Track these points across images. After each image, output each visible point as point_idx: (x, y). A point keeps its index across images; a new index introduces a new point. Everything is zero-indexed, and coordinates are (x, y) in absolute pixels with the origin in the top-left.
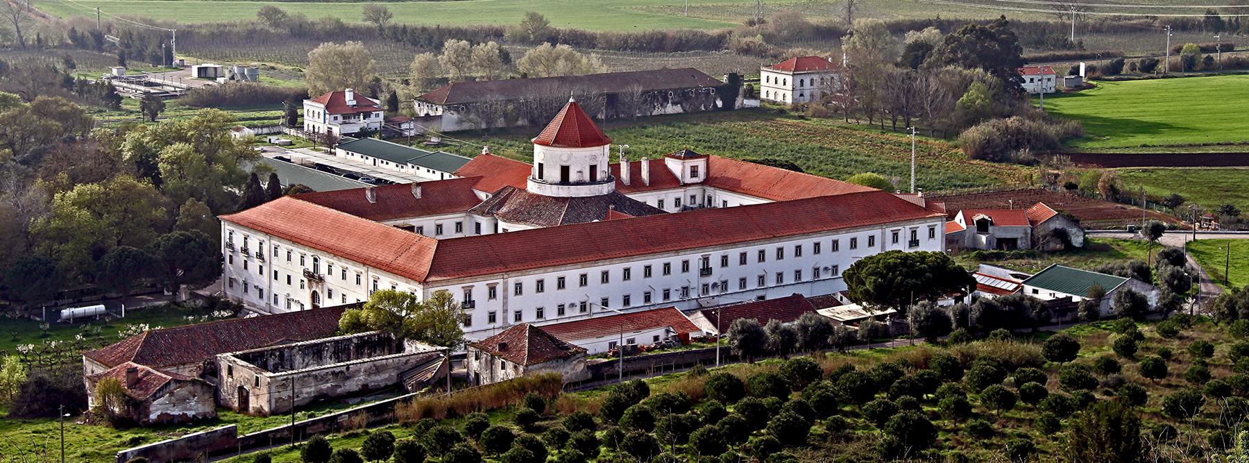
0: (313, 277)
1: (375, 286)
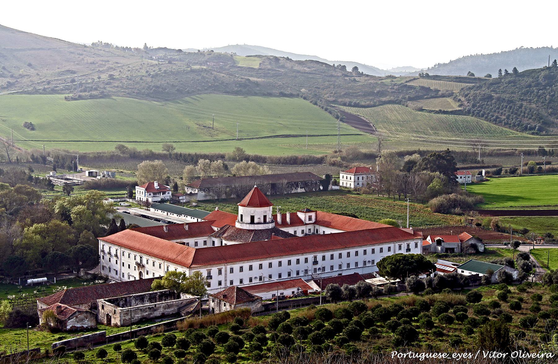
0: (140, 265)
1: (168, 269)
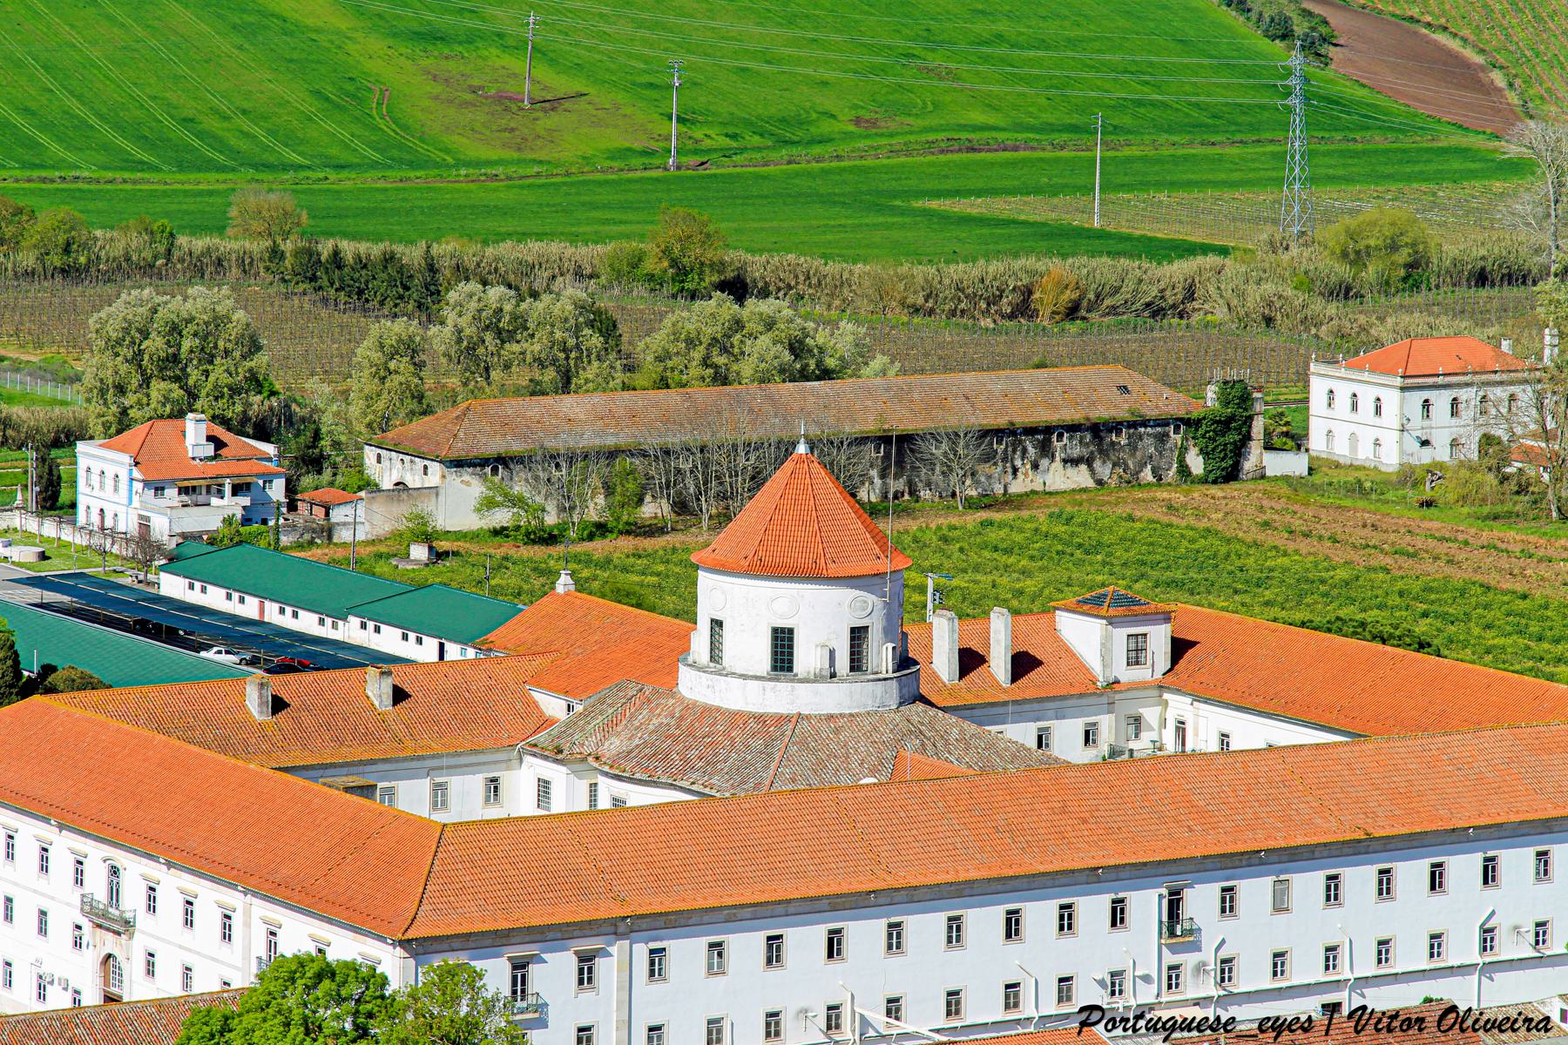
0: (110, 920)
1: (272, 946)
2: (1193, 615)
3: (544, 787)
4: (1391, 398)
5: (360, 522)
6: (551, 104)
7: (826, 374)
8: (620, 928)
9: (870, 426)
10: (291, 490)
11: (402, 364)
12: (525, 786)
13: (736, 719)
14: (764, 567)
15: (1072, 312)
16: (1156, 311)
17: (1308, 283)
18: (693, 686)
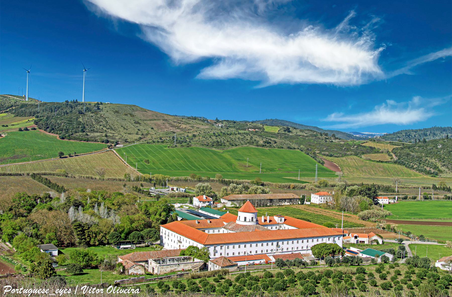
2: (287, 217)
3: (223, 231)
4: (318, 197)
5: (219, 206)
6: (249, 166)
7: (266, 193)
8: (224, 244)
9: (269, 198)
10: (213, 202)
11: (225, 191)
12: (222, 231)
13: (241, 225)
14: (244, 211)
15: (294, 188)
16: (302, 188)
17: (316, 186)
18: (238, 222)
